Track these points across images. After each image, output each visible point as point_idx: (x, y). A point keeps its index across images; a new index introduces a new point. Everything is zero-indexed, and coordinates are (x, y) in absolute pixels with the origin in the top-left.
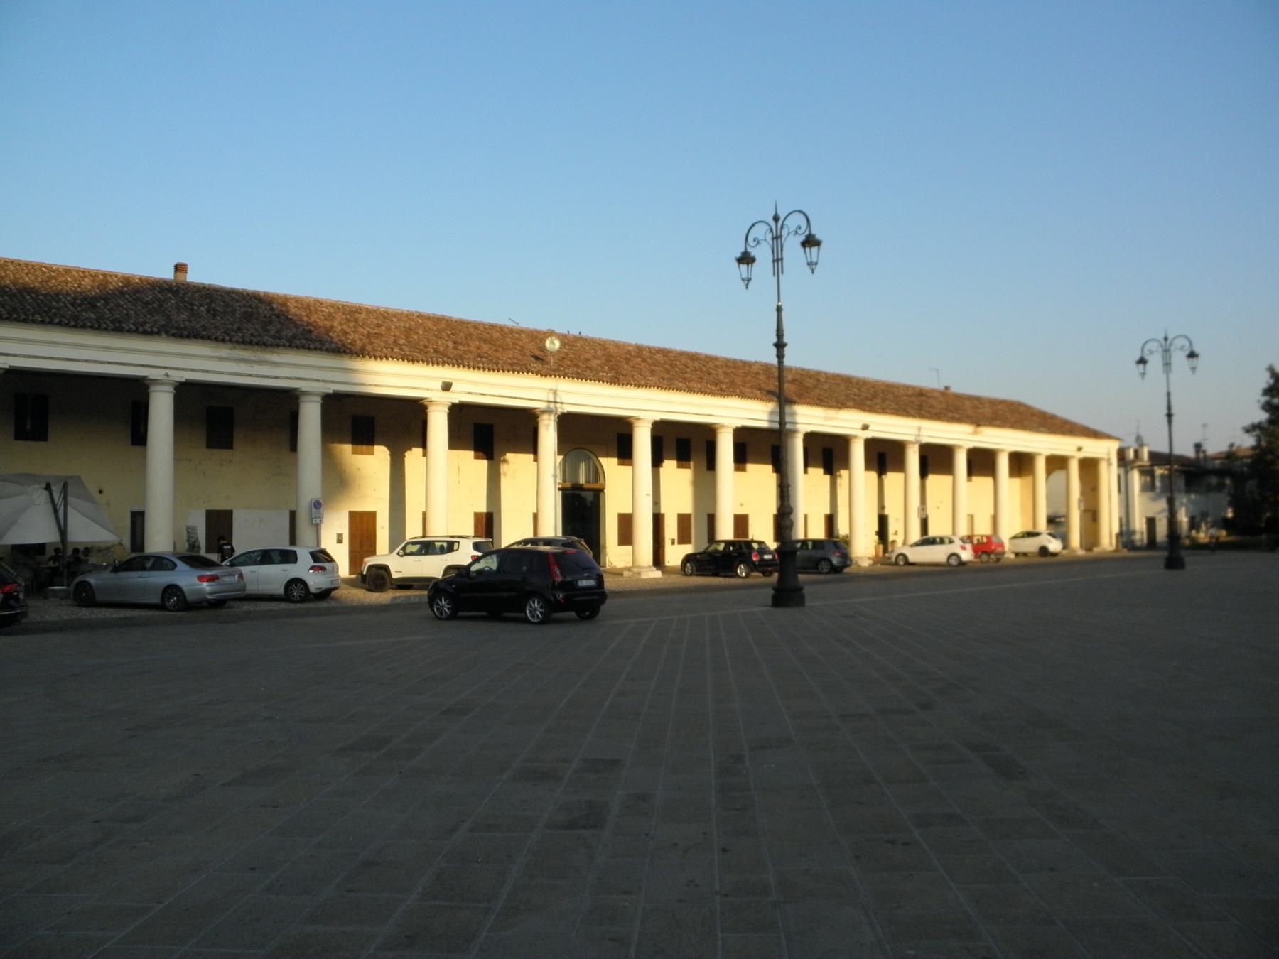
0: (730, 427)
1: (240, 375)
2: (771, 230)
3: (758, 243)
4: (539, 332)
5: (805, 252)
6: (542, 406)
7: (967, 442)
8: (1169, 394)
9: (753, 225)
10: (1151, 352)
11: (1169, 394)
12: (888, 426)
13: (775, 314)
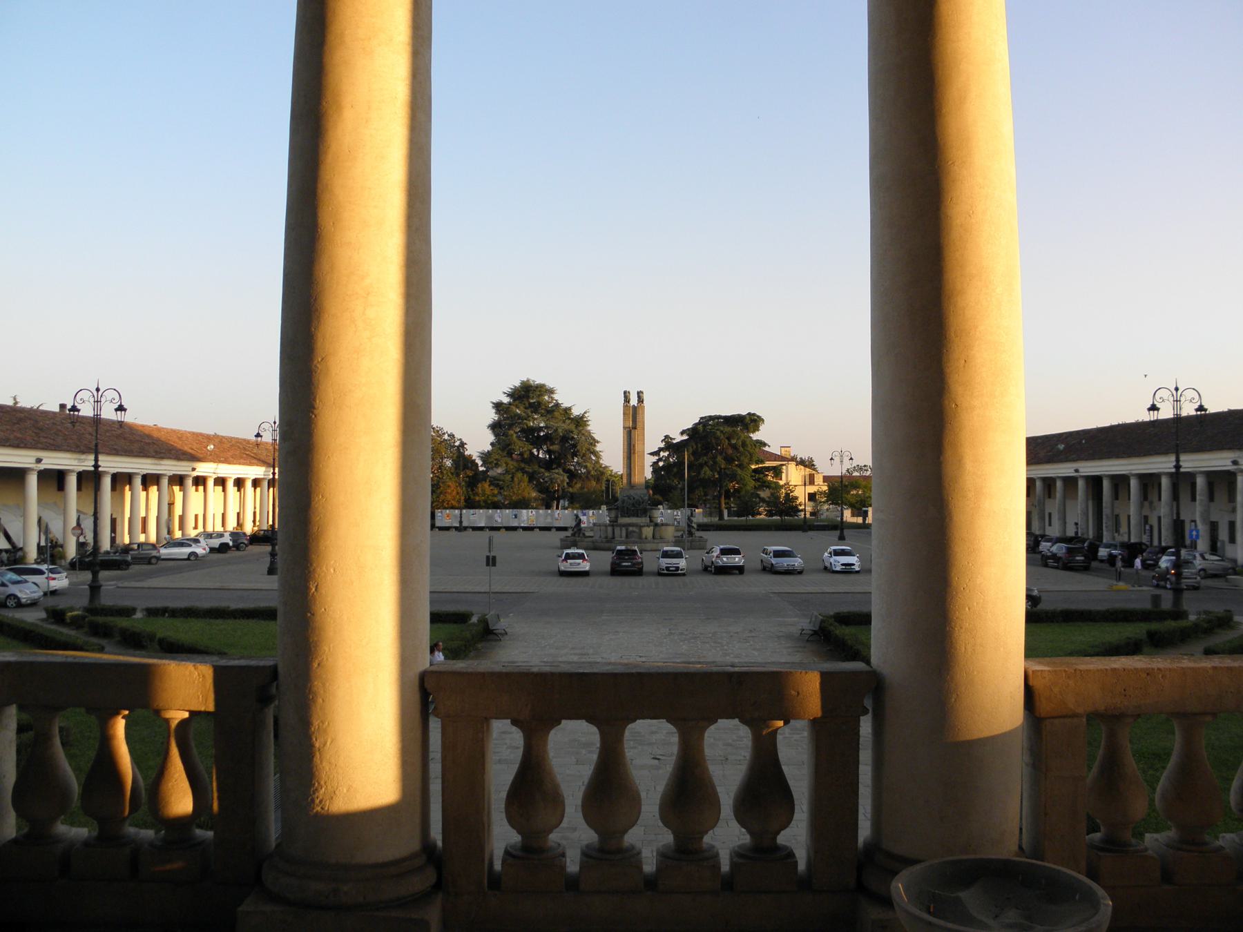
0: (36, 470)
4: (1051, 478)
6: (262, 477)
7: (143, 470)
10: (836, 456)
12: (55, 460)
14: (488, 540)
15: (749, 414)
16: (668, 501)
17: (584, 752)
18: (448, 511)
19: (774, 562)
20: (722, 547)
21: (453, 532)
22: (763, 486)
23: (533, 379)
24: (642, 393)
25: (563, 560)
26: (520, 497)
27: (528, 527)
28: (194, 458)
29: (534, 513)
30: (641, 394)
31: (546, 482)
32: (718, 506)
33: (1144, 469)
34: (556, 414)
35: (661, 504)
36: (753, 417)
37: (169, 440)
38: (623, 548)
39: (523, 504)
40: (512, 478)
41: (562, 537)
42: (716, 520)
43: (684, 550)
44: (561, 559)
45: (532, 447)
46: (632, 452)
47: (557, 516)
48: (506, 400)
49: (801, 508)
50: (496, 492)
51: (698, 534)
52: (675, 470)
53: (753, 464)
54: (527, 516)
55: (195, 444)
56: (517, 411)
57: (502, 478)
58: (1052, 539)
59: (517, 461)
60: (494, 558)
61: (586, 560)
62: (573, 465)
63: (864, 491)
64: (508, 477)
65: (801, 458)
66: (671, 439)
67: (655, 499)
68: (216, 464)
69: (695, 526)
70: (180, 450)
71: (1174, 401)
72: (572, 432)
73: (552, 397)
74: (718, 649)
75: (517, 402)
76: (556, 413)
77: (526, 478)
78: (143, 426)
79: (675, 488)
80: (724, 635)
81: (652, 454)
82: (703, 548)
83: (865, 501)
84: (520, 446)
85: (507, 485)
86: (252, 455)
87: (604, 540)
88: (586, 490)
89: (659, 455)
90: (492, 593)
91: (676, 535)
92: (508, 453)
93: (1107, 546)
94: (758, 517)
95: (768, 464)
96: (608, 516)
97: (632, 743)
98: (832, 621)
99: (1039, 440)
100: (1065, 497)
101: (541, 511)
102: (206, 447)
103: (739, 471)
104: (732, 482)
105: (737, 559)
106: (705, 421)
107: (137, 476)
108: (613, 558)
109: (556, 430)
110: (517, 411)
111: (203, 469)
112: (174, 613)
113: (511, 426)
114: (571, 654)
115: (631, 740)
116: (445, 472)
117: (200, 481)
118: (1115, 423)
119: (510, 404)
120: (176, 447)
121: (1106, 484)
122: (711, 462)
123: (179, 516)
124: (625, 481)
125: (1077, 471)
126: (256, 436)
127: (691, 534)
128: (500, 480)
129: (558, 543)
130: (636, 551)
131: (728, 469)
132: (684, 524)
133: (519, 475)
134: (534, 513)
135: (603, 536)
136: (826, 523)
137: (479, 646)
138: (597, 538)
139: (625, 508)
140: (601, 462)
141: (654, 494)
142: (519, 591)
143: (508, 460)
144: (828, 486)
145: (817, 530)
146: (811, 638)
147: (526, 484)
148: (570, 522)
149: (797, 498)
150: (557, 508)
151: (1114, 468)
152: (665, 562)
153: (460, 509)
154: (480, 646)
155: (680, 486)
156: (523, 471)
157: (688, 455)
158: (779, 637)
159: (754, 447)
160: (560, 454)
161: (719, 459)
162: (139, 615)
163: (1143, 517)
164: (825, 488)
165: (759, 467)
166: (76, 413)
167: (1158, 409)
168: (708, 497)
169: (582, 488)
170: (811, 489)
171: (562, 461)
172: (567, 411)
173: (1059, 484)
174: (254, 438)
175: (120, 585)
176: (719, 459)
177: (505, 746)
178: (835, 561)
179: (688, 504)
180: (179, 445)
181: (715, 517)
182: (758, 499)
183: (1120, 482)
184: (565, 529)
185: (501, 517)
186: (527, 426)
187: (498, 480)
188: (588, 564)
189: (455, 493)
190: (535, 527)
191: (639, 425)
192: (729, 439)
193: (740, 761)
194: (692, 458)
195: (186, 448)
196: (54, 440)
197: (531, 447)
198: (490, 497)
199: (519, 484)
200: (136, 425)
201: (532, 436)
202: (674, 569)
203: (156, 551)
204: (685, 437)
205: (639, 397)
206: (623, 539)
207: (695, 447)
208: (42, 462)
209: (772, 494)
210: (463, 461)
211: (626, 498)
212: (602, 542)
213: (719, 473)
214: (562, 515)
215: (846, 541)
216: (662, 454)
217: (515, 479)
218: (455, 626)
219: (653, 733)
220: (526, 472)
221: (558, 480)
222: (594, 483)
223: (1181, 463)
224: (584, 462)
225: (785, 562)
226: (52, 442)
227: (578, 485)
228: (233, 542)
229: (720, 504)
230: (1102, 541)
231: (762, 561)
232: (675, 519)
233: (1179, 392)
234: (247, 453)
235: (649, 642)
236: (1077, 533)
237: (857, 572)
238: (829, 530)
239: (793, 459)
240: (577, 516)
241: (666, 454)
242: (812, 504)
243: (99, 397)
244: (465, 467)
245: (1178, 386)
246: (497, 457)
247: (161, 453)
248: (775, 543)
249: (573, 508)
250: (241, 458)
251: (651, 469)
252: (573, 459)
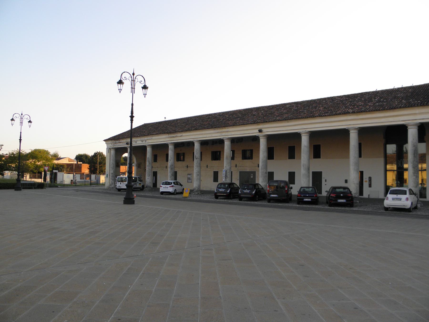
1: (369, 123)
8: (21, 133)
9: (124, 72)
11: (21, 133)
13: (131, 106)
20: (289, 146)
163: (152, 172)
236: (200, 186)
238: (35, 188)
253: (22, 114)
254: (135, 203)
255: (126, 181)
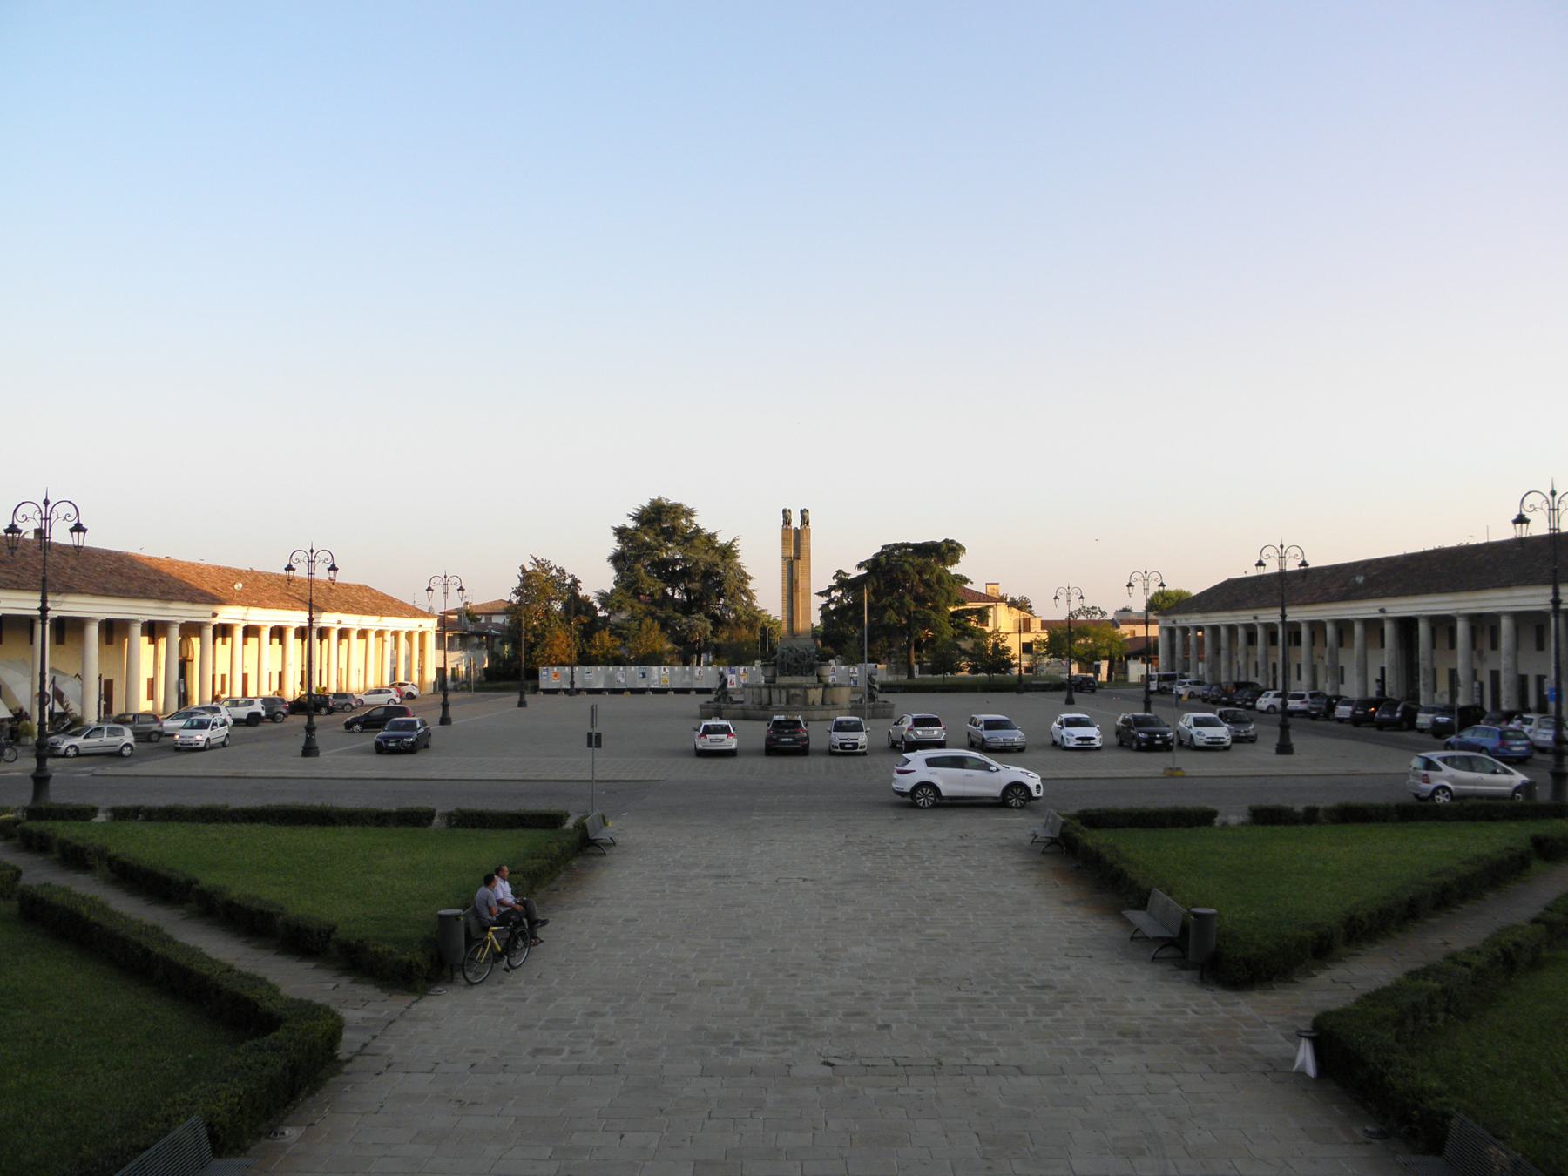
2: (1548, 502)
3: (1534, 509)
4: (1347, 621)
5: (1515, 528)
9: (1529, 493)
14: (589, 711)
15: (946, 541)
16: (841, 654)
17: (714, 1051)
18: (555, 669)
19: (985, 736)
20: (915, 715)
21: (562, 697)
22: (964, 635)
23: (666, 497)
24: (807, 511)
25: (701, 735)
26: (649, 650)
27: (659, 689)
28: (215, 600)
29: (667, 670)
30: (805, 514)
31: (684, 630)
32: (906, 660)
33: (1476, 608)
34: (696, 542)
35: (833, 659)
36: (950, 546)
37: (184, 577)
38: (782, 718)
39: (653, 659)
40: (640, 625)
41: (702, 703)
42: (904, 678)
43: (863, 718)
44: (698, 734)
45: (665, 585)
46: (794, 589)
47: (697, 674)
48: (631, 524)
49: (1014, 662)
50: (618, 644)
51: (882, 697)
52: (851, 614)
53: (951, 606)
54: (659, 675)
55: (219, 581)
56: (646, 538)
57: (626, 625)
58: (1353, 701)
59: (646, 603)
60: (599, 736)
61: (732, 735)
62: (719, 609)
63: (1095, 641)
64: (634, 625)
65: (1012, 598)
66: (845, 574)
67: (824, 652)
68: (245, 608)
69: (877, 686)
70: (198, 589)
71: (1550, 510)
72: (717, 565)
73: (690, 521)
74: (916, 866)
75: (645, 527)
76: (695, 541)
77: (657, 625)
78: (150, 558)
79: (851, 638)
80: (923, 844)
81: (821, 594)
82: (889, 716)
83: (1096, 652)
84: (651, 584)
85: (633, 634)
86: (297, 596)
87: (758, 706)
88: (734, 640)
89: (830, 595)
90: (597, 781)
91: (854, 699)
92: (634, 593)
93: (1428, 711)
94: (960, 674)
95: (970, 605)
96: (763, 674)
97: (789, 1033)
98: (1077, 823)
99: (1327, 572)
100: (1365, 646)
101: (676, 668)
102: (233, 587)
103: (934, 615)
104: (924, 629)
105: (936, 733)
106: (889, 551)
107: (136, 625)
108: (768, 731)
109: (696, 563)
110: (646, 538)
111: (227, 614)
112: (151, 815)
113: (638, 558)
114: (705, 877)
115: (788, 1028)
116: (552, 618)
117: (224, 631)
118: (1429, 547)
119: (636, 529)
120: (191, 586)
121: (1423, 629)
122: (898, 604)
123: (149, 679)
124: (785, 627)
125: (1382, 611)
126: (286, 569)
127: (872, 698)
128: (623, 629)
129: (697, 712)
130: (799, 722)
131: (920, 612)
132: (863, 684)
133: (648, 621)
134: (667, 670)
135: (756, 701)
136: (1047, 682)
137: (574, 863)
138: (748, 703)
139: (786, 664)
140: (755, 604)
141: (823, 645)
142: (639, 778)
143: (635, 601)
144: (1049, 633)
145: (1036, 691)
146: (1048, 850)
147: (657, 632)
148: (714, 683)
149: (1009, 649)
150: (698, 664)
151: (1529, 601)
152: (838, 737)
153: (572, 665)
154: (574, 864)
155: (856, 635)
156: (653, 616)
157: (868, 595)
158: (1001, 847)
159: (952, 584)
160: (701, 594)
161: (908, 599)
162: (101, 818)
164: (1044, 636)
165: (958, 610)
166: (17, 535)
167: (1527, 521)
168: (894, 649)
169: (730, 638)
170: (1027, 638)
171: (705, 603)
172: (711, 538)
173: (1358, 629)
174: (284, 572)
175: (99, 772)
176: (908, 599)
177: (592, 1041)
178: (1068, 734)
179: (868, 658)
180: (196, 582)
181: (903, 674)
182: (957, 652)
183: (1443, 625)
184: (708, 691)
185: (625, 676)
186: (658, 557)
187: (620, 628)
188: (735, 740)
189: (564, 645)
190: (669, 690)
191: (803, 554)
192: (920, 573)
193: (961, 1066)
194: (873, 599)
195: (207, 588)
196: (18, 576)
197: (663, 585)
198: (611, 651)
199: (648, 632)
200: (140, 557)
201: (664, 570)
202: (850, 746)
203: (157, 725)
204: (863, 572)
205: (803, 517)
206: (783, 705)
207: (876, 584)
208: (218, 616)
209: (975, 644)
210: (577, 606)
211: (786, 651)
212: (755, 709)
213: (908, 618)
214: (704, 674)
215: (1075, 706)
216: (833, 594)
217: (644, 627)
218: (543, 832)
219: (823, 1014)
220: (658, 618)
221: (699, 628)
222: (745, 631)
223: (1561, 597)
224: (733, 604)
225: (1000, 736)
226: (15, 579)
227: (725, 635)
228: (266, 712)
229: (909, 656)
230: (1418, 703)
231: (969, 733)
232: (851, 678)
233: (1284, 550)
234: (290, 593)
235: (817, 857)
237: (1098, 749)
238: (1051, 691)
239: (1002, 599)
240: (722, 675)
241: (839, 594)
242: (1028, 656)
243: (48, 512)
244: (578, 612)
245: (1555, 489)
246: (620, 598)
247: (169, 593)
248: (988, 709)
249: (719, 664)
250: (282, 600)
251: (819, 614)
252: (719, 600)
253: (1146, 573)
254: (1295, 751)
255: (122, 729)
